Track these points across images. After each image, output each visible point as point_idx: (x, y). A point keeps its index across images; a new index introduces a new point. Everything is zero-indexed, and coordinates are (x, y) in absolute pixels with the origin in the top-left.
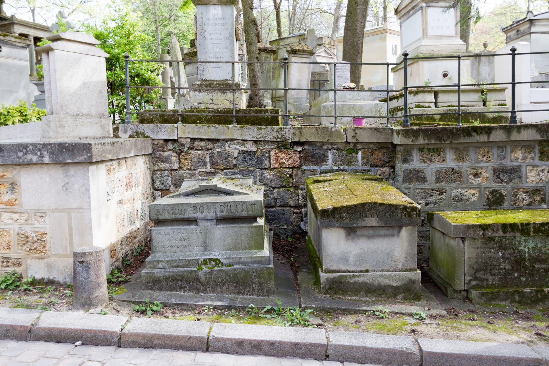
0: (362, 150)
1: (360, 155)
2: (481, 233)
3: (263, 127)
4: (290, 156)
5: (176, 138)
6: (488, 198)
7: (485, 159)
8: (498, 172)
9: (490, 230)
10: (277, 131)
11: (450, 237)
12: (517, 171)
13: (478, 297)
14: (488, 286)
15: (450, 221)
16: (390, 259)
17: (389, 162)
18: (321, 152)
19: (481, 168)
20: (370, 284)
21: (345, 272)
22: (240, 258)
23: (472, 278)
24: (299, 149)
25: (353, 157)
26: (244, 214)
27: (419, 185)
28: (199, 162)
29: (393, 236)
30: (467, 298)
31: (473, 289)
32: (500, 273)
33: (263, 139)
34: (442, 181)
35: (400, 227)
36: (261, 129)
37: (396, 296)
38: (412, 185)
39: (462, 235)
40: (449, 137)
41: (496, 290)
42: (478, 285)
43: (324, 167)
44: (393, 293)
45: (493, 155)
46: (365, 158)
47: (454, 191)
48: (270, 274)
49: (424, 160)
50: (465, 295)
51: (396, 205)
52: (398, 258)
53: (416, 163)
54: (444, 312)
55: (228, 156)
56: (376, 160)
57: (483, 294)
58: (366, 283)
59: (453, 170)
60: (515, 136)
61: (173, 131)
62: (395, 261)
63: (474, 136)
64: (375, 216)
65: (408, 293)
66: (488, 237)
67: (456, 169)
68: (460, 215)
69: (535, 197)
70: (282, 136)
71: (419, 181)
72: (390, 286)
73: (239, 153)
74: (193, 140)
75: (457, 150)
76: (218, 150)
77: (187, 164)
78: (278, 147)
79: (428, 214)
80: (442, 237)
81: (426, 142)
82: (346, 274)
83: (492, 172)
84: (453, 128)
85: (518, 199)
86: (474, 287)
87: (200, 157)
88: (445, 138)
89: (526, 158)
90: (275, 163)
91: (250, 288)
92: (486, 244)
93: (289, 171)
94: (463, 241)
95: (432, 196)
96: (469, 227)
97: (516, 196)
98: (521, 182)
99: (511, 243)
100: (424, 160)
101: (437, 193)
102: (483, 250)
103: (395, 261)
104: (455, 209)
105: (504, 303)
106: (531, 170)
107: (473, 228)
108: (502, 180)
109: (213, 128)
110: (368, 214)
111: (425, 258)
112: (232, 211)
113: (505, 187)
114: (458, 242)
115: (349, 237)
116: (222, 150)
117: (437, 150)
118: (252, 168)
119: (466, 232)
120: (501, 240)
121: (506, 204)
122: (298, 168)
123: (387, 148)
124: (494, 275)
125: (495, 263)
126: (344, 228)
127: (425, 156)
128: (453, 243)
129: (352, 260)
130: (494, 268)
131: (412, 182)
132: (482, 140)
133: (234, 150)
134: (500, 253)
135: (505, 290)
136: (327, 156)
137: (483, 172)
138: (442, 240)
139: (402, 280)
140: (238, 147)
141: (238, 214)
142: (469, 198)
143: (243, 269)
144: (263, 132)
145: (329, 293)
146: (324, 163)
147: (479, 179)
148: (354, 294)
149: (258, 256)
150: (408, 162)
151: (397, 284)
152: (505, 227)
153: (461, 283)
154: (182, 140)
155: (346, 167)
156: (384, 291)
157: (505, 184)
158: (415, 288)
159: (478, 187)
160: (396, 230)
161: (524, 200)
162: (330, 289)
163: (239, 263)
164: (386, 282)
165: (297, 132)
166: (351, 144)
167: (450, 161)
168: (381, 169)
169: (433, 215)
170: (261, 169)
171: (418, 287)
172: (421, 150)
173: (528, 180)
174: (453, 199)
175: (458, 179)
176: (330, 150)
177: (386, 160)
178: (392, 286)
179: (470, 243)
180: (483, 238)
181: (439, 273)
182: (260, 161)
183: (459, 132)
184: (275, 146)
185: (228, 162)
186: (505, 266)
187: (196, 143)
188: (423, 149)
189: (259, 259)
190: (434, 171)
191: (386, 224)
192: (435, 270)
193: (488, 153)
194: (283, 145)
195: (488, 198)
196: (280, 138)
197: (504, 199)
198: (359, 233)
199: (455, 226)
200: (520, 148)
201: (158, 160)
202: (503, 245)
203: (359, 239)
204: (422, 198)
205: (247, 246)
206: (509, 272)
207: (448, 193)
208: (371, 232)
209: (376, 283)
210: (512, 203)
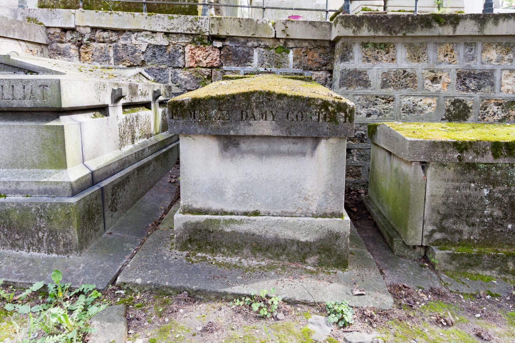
0: (294, 49)
1: (291, 55)
2: (456, 156)
3: (175, 16)
4: (207, 53)
5: (73, 26)
6: (448, 110)
7: (447, 59)
8: (463, 77)
9: (471, 152)
10: (192, 21)
11: (401, 159)
12: (489, 76)
13: (445, 261)
14: (462, 243)
15: (403, 135)
16: (297, 195)
17: (326, 65)
18: (245, 50)
19: (442, 71)
20: (261, 236)
21: (217, 214)
22: (18, 183)
23: (435, 228)
24: (219, 44)
25: (283, 57)
26: (28, 104)
27: (360, 90)
28: (101, 56)
29: (304, 154)
30: (425, 258)
31: (437, 245)
32: (483, 222)
33: (174, 31)
34: (389, 86)
35: (317, 140)
36: (173, 18)
37: (304, 258)
38: (351, 89)
39: (422, 158)
40: (402, 28)
41: (475, 251)
42: (445, 239)
43: (248, 69)
44: (299, 253)
45: (459, 54)
46: (297, 58)
47: (405, 99)
48: (68, 215)
49: (367, 58)
50: (423, 253)
51: (309, 99)
52: (310, 194)
53: (357, 61)
54: (388, 301)
55: (135, 51)
56: (310, 62)
57: (453, 257)
58: (254, 235)
59: (405, 72)
60: (490, 29)
61: (69, 17)
62: (306, 199)
63: (435, 27)
64: (270, 118)
65: (327, 254)
66: (467, 163)
67: (409, 71)
68: (418, 127)
69: (511, 111)
70: (197, 28)
71: (360, 85)
72: (293, 242)
73: (148, 47)
74: (94, 29)
75: (410, 46)
76: (124, 43)
77: (87, 58)
78: (193, 42)
79: (369, 127)
80: (388, 159)
81: (372, 33)
82: (217, 217)
83: (456, 77)
84: (408, 15)
85: (488, 112)
86: (438, 243)
87: (103, 51)
88: (397, 29)
89: (502, 59)
90: (191, 61)
91: (33, 237)
92: (463, 174)
93: (207, 72)
94: (423, 167)
95: (376, 104)
96: (434, 145)
97: (485, 109)
98: (493, 90)
99: (505, 175)
100: (367, 58)
101: (383, 101)
102: (457, 184)
103: (306, 199)
104: (405, 121)
105: (488, 273)
106: (507, 76)
107: (443, 147)
108: (468, 88)
109: (116, 15)
110: (256, 113)
111: (358, 202)
112: (6, 96)
113: (471, 97)
114: (416, 168)
115: (225, 153)
116: (128, 42)
117: (385, 45)
118: (163, 66)
119: (431, 154)
120: (489, 169)
121: (472, 117)
122: (218, 68)
123: (324, 47)
124: (473, 225)
125: (475, 206)
126: (218, 137)
127: (369, 53)
128: (405, 168)
129: (230, 193)
130: (473, 214)
131: (350, 86)
132: (446, 34)
133: (142, 43)
134: (485, 190)
135: (490, 251)
136: (252, 55)
137: (444, 75)
138: (388, 163)
139: (317, 232)
140: (146, 40)
141: (15, 104)
142: (424, 109)
143: (19, 204)
144: (175, 21)
145: (187, 249)
146: (249, 63)
147: (437, 85)
148: (232, 251)
149: (51, 180)
150: (347, 60)
151: (308, 239)
152: (497, 147)
153: (416, 234)
154: (81, 29)
155: (274, 69)
156: (284, 250)
157: (472, 93)
158: (339, 246)
159: (436, 95)
160: (309, 145)
161: (495, 114)
162: (190, 241)
163: (16, 192)
164: (288, 234)
165: (216, 23)
166: (281, 41)
167: (402, 59)
168: (316, 73)
169: (375, 126)
170: (174, 68)
171: (344, 246)
172: (364, 45)
173: (502, 89)
174: (403, 110)
175: (411, 84)
176: (256, 47)
177: (323, 62)
178: (298, 242)
179: (436, 171)
180: (459, 164)
181: (380, 208)
182: (172, 58)
183: (416, 22)
184: (190, 40)
185: (135, 58)
186: (492, 212)
187: (98, 34)
188: (367, 43)
189: (53, 187)
190: (380, 73)
191: (290, 133)
192: (375, 201)
193: (452, 51)
194: (200, 39)
195: (448, 110)
196: (195, 31)
197: (469, 111)
198: (244, 146)
199: (413, 143)
200: (494, 46)
201: (55, 52)
202: (492, 178)
203: (243, 157)
204: (363, 107)
205: (37, 161)
206: (499, 222)
207: (397, 101)
208: (264, 146)
209: (271, 235)
210: (479, 117)
